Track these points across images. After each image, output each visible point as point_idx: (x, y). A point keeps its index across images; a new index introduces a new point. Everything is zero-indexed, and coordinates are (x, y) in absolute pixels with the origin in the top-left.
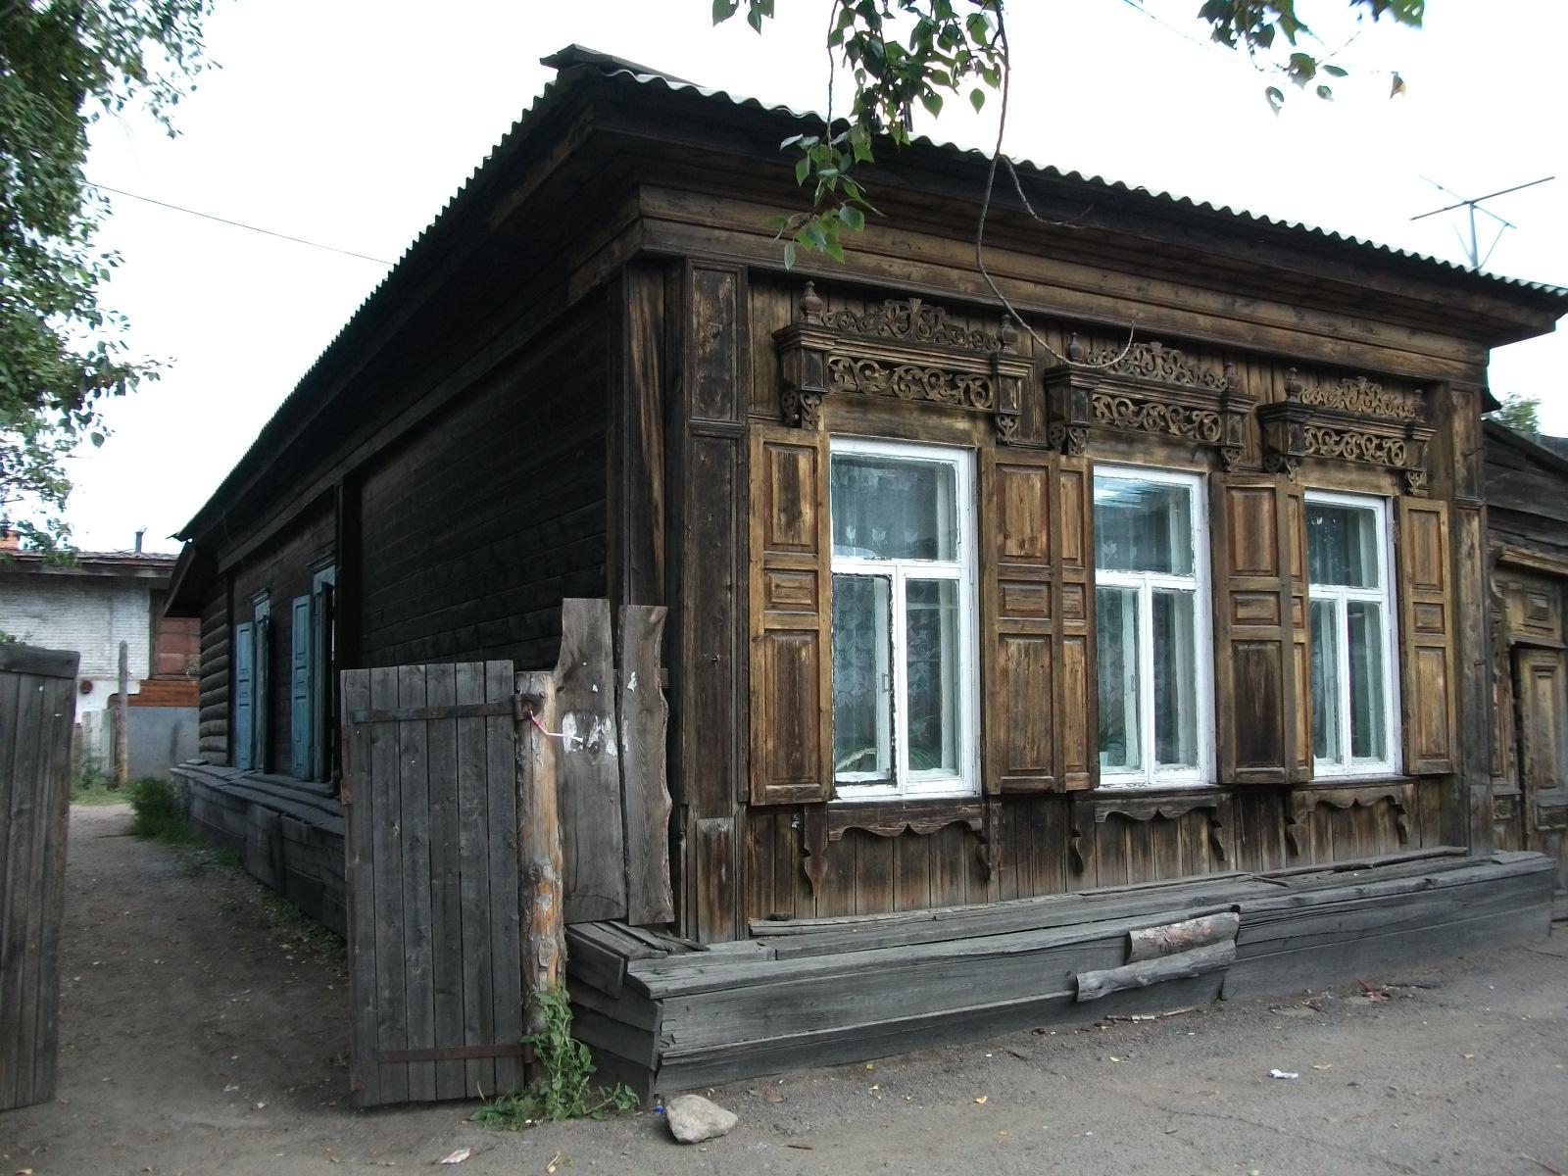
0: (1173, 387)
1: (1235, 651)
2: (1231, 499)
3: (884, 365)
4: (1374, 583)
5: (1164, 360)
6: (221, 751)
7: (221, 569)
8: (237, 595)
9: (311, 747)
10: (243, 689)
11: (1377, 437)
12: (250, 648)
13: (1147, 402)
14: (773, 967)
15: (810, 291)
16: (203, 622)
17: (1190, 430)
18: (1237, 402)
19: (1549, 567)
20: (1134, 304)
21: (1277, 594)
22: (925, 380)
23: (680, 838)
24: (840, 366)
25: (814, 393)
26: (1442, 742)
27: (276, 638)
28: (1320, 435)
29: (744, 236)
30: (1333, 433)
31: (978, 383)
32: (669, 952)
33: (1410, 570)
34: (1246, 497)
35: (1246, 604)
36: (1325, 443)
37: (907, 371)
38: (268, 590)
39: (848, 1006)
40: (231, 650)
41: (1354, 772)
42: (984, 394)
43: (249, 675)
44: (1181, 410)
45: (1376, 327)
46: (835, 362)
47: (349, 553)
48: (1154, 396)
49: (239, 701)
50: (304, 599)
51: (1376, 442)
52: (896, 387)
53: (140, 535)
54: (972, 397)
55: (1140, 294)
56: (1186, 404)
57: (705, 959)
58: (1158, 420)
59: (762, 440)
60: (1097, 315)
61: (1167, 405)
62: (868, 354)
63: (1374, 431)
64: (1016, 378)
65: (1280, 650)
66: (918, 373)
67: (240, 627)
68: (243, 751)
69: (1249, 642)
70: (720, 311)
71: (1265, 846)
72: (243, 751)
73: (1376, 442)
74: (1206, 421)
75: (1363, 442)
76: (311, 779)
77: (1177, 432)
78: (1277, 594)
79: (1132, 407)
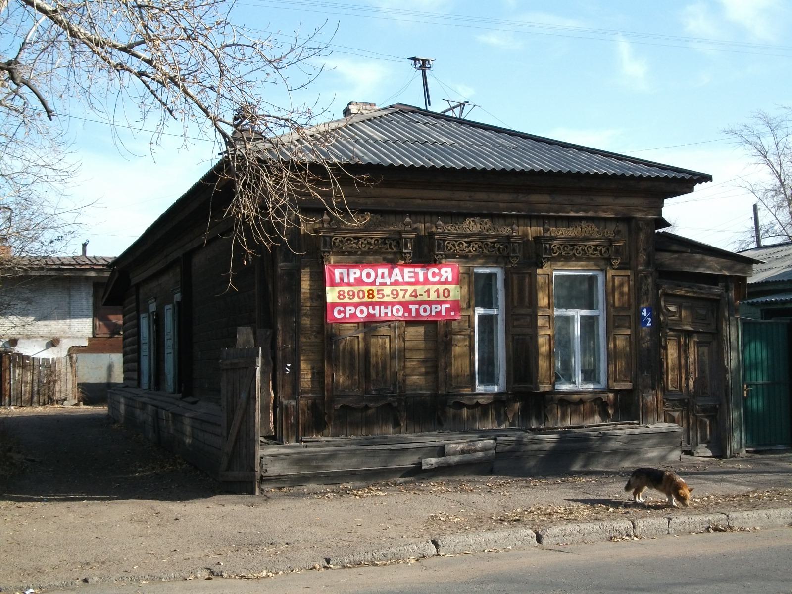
1: (513, 338)
3: (355, 238)
5: (481, 224)
6: (134, 380)
7: (132, 284)
8: (141, 297)
11: (594, 245)
12: (147, 326)
15: (325, 215)
16: (124, 317)
19: (703, 296)
20: (467, 203)
21: (531, 316)
22: (373, 242)
24: (338, 240)
25: (327, 251)
27: (158, 322)
30: (569, 246)
33: (612, 302)
35: (517, 320)
36: (565, 251)
37: (365, 240)
38: (156, 298)
40: (138, 326)
43: (147, 341)
44: (489, 243)
46: (336, 239)
47: (186, 287)
48: (475, 239)
49: (142, 354)
51: (593, 247)
52: (360, 246)
53: (84, 245)
54: (393, 247)
61: (482, 242)
62: (348, 235)
63: (592, 243)
64: (411, 239)
66: (370, 240)
67: (142, 316)
68: (145, 380)
69: (519, 335)
72: (145, 380)
75: (586, 248)
76: (174, 393)
78: (531, 316)
79: (465, 244)
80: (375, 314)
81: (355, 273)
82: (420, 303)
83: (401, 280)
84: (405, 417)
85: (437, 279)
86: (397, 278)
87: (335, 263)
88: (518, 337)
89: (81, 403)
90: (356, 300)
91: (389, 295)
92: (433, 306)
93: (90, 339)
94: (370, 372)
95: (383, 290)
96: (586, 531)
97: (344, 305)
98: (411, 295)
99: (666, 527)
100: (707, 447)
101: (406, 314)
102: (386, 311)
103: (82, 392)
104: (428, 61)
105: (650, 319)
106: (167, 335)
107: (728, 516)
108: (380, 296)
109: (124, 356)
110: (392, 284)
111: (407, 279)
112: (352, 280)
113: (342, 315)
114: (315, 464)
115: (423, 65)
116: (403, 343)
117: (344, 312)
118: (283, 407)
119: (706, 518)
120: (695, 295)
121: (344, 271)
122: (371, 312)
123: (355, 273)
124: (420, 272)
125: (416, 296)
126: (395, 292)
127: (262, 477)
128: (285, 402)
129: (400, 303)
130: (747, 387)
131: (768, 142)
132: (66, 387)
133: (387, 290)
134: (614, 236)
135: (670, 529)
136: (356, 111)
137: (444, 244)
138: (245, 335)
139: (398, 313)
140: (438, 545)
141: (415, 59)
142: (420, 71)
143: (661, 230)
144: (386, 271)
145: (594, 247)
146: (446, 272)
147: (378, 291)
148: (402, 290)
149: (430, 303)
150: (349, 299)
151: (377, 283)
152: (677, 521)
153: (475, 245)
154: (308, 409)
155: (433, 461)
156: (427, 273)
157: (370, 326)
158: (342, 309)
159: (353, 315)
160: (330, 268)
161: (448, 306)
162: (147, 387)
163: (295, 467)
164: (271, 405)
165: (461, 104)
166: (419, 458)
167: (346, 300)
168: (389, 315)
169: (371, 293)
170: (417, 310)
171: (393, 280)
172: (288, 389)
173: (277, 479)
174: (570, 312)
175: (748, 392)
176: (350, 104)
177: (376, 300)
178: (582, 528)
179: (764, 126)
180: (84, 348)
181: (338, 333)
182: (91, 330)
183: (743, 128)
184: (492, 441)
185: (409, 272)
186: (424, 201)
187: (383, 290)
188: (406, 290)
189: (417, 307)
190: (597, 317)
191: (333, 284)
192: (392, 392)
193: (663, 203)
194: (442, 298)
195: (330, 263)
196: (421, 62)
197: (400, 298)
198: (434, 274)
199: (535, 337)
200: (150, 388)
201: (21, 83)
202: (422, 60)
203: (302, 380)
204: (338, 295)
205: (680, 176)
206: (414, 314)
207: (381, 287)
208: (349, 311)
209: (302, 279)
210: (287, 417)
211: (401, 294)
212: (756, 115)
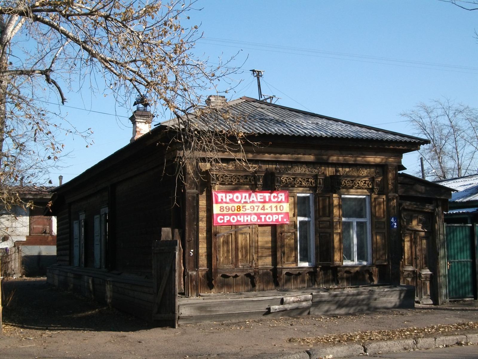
1: (319, 235)
2: (319, 199)
4: (366, 217)
9: (101, 259)
10: (76, 243)
11: (364, 181)
14: (203, 301)
21: (330, 221)
23: (185, 276)
24: (220, 177)
31: (253, 177)
32: (182, 298)
37: (235, 176)
38: (85, 211)
39: (218, 309)
44: (306, 179)
46: (219, 176)
50: (98, 216)
51: (363, 182)
54: (251, 181)
57: (189, 299)
60: (284, 159)
61: (302, 178)
64: (262, 176)
65: (330, 234)
66: (238, 177)
68: (76, 261)
69: (323, 233)
70: (194, 167)
80: (241, 221)
81: (230, 196)
82: (267, 214)
83: (256, 200)
84: (258, 282)
85: (276, 199)
86: (253, 199)
87: (219, 189)
88: (322, 234)
89: (24, 276)
90: (230, 212)
91: (248, 209)
92: (274, 216)
93: (27, 237)
94: (238, 255)
95: (245, 206)
96: (391, 346)
97: (224, 215)
98: (261, 209)
99: (434, 343)
100: (430, 298)
101: (259, 221)
102: (247, 218)
103: (24, 269)
104: (261, 72)
105: (395, 224)
106: (96, 233)
107: (467, 336)
108: (244, 210)
109: (57, 247)
110: (251, 202)
111: (259, 200)
112: (228, 201)
113: (222, 221)
114: (209, 309)
115: (258, 75)
116: (257, 238)
117: (224, 219)
118: (189, 275)
119: (455, 338)
120: (420, 210)
121: (224, 195)
122: (239, 219)
123: (230, 196)
124: (267, 195)
125: (264, 210)
126: (252, 207)
127: (179, 317)
128: (190, 273)
129: (256, 214)
130: (449, 263)
131: (426, 121)
132: (15, 265)
133: (248, 206)
134: (375, 175)
135: (436, 344)
136: (214, 101)
137: (280, 179)
138: (166, 232)
139: (254, 219)
140: (311, 354)
141: (254, 71)
142: (256, 78)
143: (400, 172)
144: (247, 195)
145: (364, 182)
146: (281, 196)
147: (243, 206)
148: (256, 206)
149: (272, 214)
150: (226, 211)
151: (242, 202)
152: (439, 339)
153: (298, 180)
154: (202, 277)
155: (277, 307)
156: (270, 196)
157: (236, 228)
158: (222, 217)
159: (229, 221)
160: (215, 193)
161: (282, 216)
162: (78, 265)
163: (198, 311)
164: (182, 274)
165: (271, 97)
166: (269, 306)
167: (225, 212)
168: (249, 221)
169: (239, 208)
170: (265, 218)
171: (251, 200)
172: (192, 265)
173: (188, 318)
174: (350, 220)
175: (450, 266)
176: (211, 96)
177: (241, 212)
178: (389, 344)
179: (423, 112)
180: (24, 242)
181: (220, 231)
182: (29, 231)
183: (412, 113)
184: (310, 296)
185: (260, 196)
187: (245, 206)
188: (259, 207)
189: (265, 216)
190: (365, 223)
191: (217, 202)
192: (251, 267)
193: (402, 156)
194: (279, 211)
195: (215, 190)
196: (257, 73)
197: (255, 211)
198: (274, 197)
199: (331, 235)
200: (79, 266)
201: (51, 83)
202: (258, 71)
203: (200, 259)
204: (220, 209)
205: (413, 140)
206: (263, 220)
207: (244, 205)
208: (227, 218)
209: (200, 199)
210: (191, 281)
211: (256, 208)
212: (419, 105)
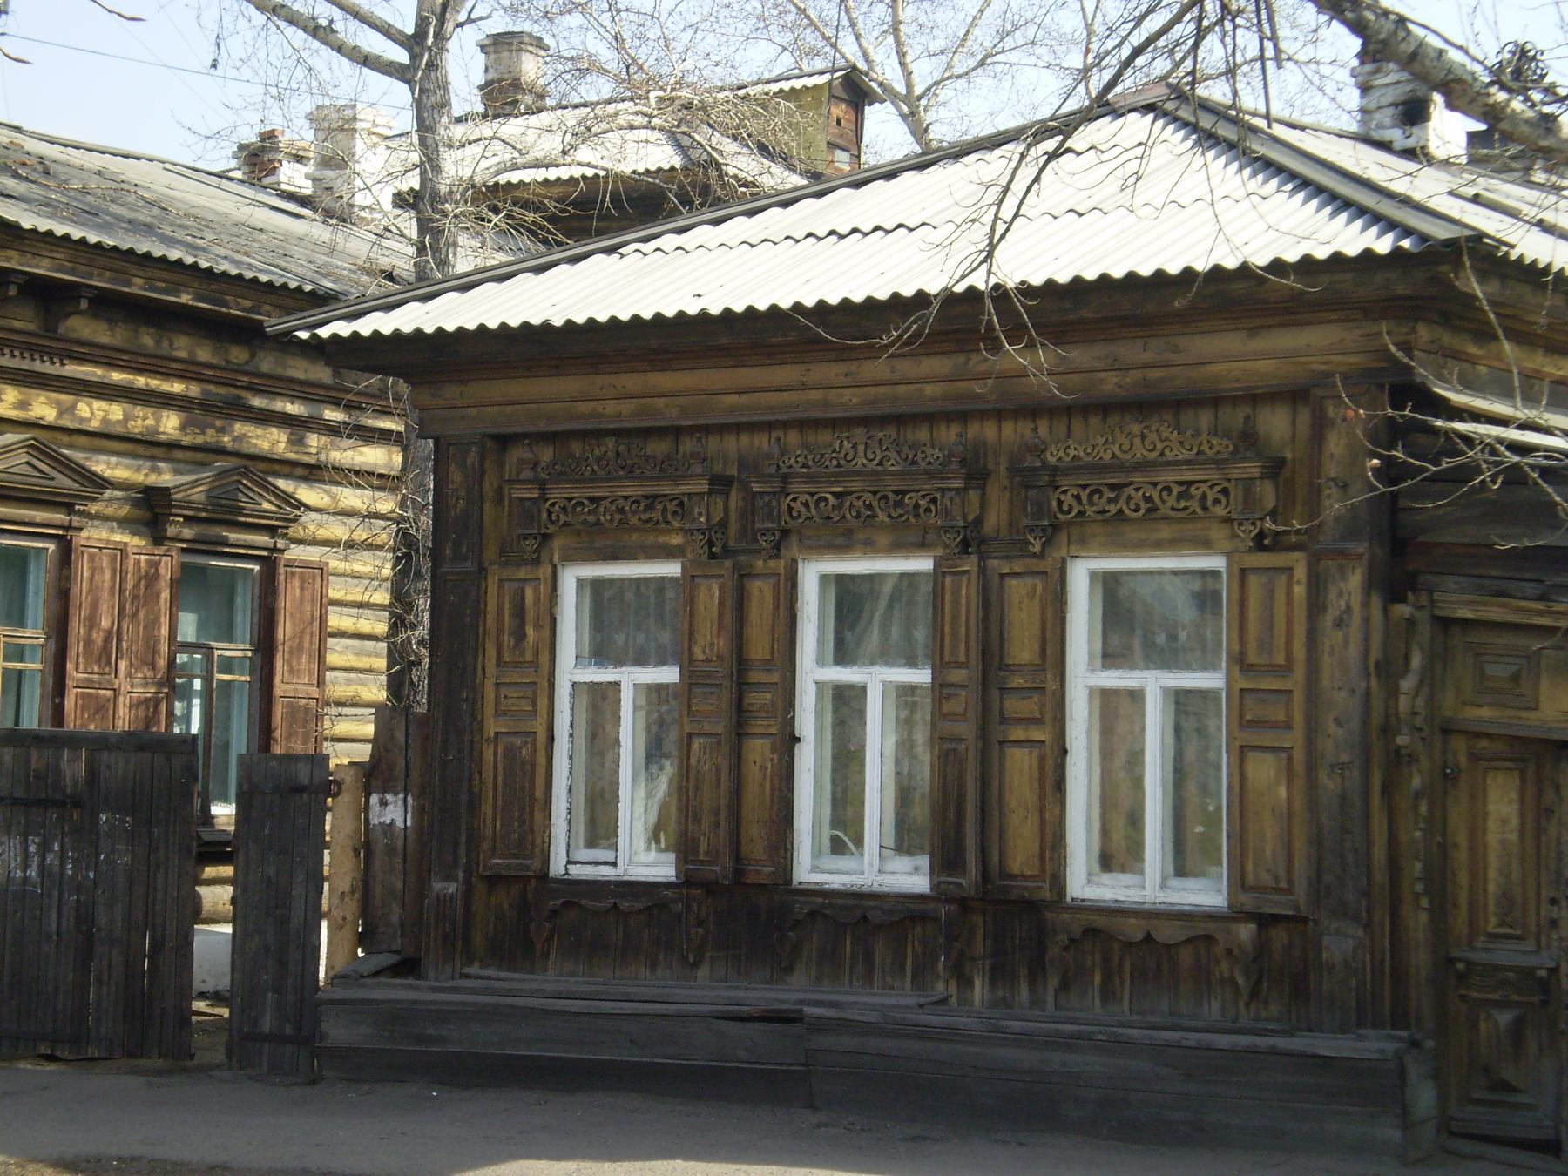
0: (875, 473)
3: (592, 500)
4: (820, 685)
11: (1181, 483)
13: (851, 493)
17: (901, 516)
18: (943, 479)
26: (1282, 874)
28: (1084, 496)
29: (489, 409)
31: (675, 502)
34: (109, 700)
36: (1091, 503)
41: (1161, 900)
42: (680, 511)
45: (1182, 341)
46: (553, 505)
48: (856, 486)
51: (1176, 489)
55: (849, 378)
56: (895, 488)
58: (863, 510)
59: (497, 578)
61: (875, 493)
63: (1168, 477)
66: (621, 502)
71: (1024, 971)
73: (1176, 489)
74: (921, 502)
77: (887, 519)
186: (745, 397)
